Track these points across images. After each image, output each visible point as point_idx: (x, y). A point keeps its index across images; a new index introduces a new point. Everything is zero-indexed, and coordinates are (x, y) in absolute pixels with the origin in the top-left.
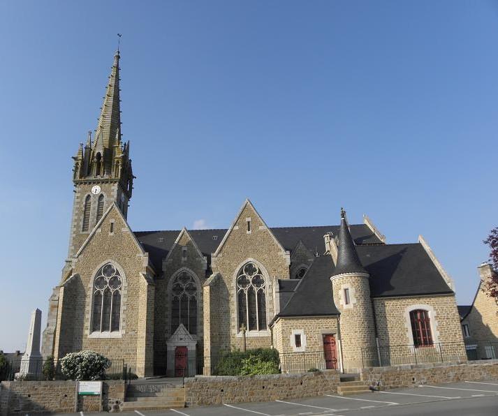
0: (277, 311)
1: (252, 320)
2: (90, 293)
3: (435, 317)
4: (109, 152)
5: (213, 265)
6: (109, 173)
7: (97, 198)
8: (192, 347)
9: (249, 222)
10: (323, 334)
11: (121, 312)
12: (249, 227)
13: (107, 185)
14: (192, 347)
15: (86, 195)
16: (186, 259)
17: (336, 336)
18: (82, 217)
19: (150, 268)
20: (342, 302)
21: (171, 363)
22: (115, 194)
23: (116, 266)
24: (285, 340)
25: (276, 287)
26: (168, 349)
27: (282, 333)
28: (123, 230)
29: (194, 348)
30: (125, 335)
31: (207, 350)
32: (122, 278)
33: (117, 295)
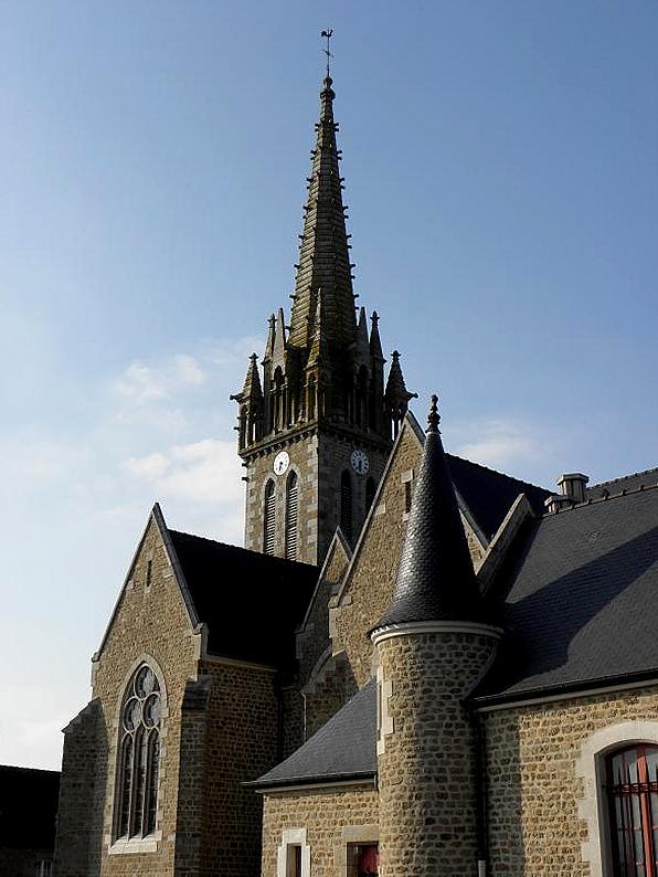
2: (114, 742)
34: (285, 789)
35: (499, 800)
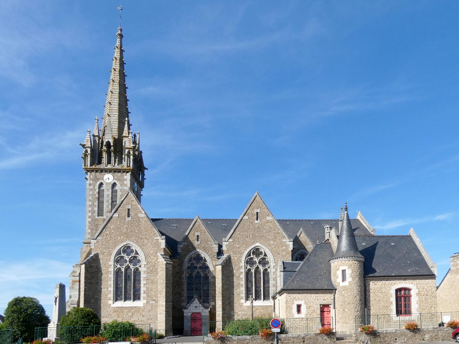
0: (280, 286)
3: (417, 294)
4: (118, 142)
5: (224, 248)
6: (120, 162)
7: (111, 186)
8: (206, 313)
9: (257, 213)
10: (321, 305)
11: (142, 285)
13: (119, 174)
14: (206, 313)
15: (99, 183)
18: (96, 203)
19: (167, 250)
20: (340, 279)
21: (187, 325)
22: (128, 183)
23: (135, 247)
24: (288, 308)
25: (280, 267)
26: (185, 315)
27: (286, 303)
28: (140, 215)
29: (208, 314)
32: (141, 257)
33: (137, 273)
34: (303, 291)
35: (323, 296)
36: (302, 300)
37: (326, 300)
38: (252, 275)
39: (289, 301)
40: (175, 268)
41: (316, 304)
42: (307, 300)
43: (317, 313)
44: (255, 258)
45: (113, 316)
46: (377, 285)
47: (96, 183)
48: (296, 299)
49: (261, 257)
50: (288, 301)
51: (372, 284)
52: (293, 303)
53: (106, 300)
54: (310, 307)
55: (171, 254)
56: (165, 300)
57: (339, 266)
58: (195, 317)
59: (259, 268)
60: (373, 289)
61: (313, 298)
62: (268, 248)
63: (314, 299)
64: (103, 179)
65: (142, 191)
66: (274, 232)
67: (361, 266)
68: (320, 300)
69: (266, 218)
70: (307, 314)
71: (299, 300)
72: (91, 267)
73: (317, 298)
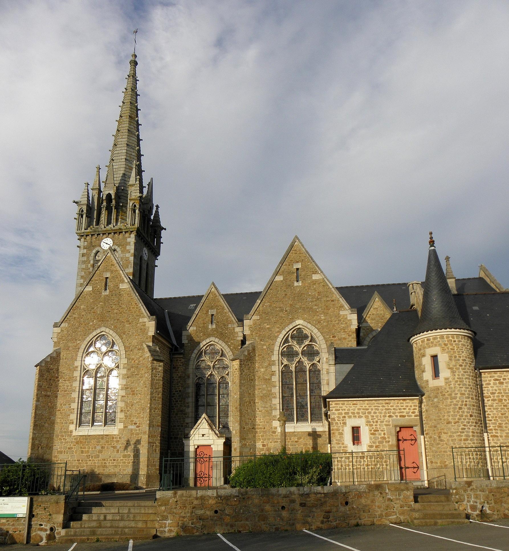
1: (301, 407)
9: (297, 269)
10: (396, 426)
12: (297, 277)
15: (94, 251)
16: (214, 326)
17: (417, 429)
20: (428, 375)
22: (131, 248)
29: (221, 448)
30: (123, 430)
31: (235, 449)
36: (361, 417)
37: (407, 417)
38: (292, 376)
39: (336, 419)
40: (178, 370)
41: (386, 425)
42: (370, 418)
43: (390, 443)
44: (296, 346)
45: (74, 451)
46: (505, 384)
47: (92, 250)
48: (350, 414)
49: (306, 344)
50: (335, 420)
51: (494, 383)
52: (345, 424)
53: (66, 423)
54: (375, 431)
55: (171, 347)
56: (148, 422)
57: (424, 348)
58: (202, 453)
59: (302, 362)
60: (497, 392)
61: (381, 413)
62: (317, 326)
63: (383, 414)
64: (100, 246)
65: (157, 259)
66: (325, 299)
67: (468, 346)
68: (395, 417)
69: (312, 277)
70: (370, 444)
71: (355, 417)
72: (48, 370)
73: (389, 413)
